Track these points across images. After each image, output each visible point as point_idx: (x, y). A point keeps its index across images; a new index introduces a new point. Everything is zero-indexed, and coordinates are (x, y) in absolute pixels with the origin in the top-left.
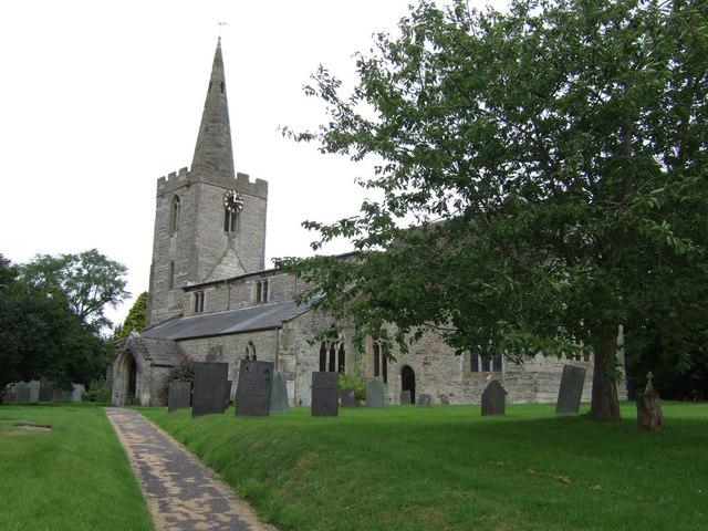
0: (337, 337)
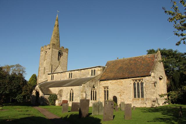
0: (95, 88)
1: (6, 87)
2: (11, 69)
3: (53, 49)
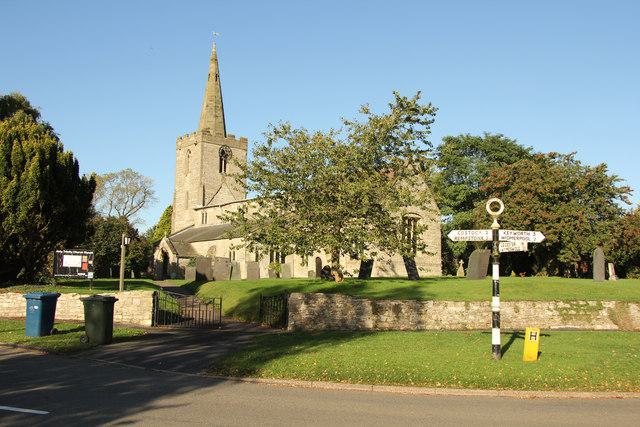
1: (100, 245)
2: (107, 185)
3: (205, 145)
